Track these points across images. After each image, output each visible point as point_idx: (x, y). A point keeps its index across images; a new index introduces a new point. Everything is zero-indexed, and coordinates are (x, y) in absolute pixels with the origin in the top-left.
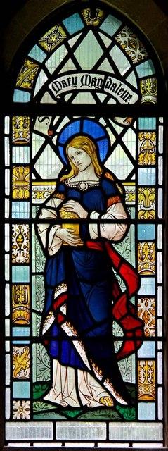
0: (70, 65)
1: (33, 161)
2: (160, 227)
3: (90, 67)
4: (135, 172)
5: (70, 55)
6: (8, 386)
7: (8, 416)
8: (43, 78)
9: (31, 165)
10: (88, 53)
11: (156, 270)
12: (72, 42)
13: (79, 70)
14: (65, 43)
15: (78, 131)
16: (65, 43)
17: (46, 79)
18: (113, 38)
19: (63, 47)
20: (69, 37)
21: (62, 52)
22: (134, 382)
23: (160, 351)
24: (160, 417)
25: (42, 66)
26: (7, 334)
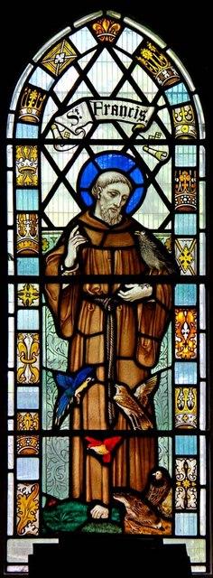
0: (83, 90)
1: (43, 205)
4: (171, 218)
5: (83, 76)
7: (10, 532)
8: (51, 108)
9: (40, 213)
11: (60, 41)
12: (83, 63)
13: (96, 96)
14: (75, 64)
16: (75, 64)
17: (55, 109)
19: (72, 69)
20: (80, 56)
21: (72, 75)
24: (203, 532)
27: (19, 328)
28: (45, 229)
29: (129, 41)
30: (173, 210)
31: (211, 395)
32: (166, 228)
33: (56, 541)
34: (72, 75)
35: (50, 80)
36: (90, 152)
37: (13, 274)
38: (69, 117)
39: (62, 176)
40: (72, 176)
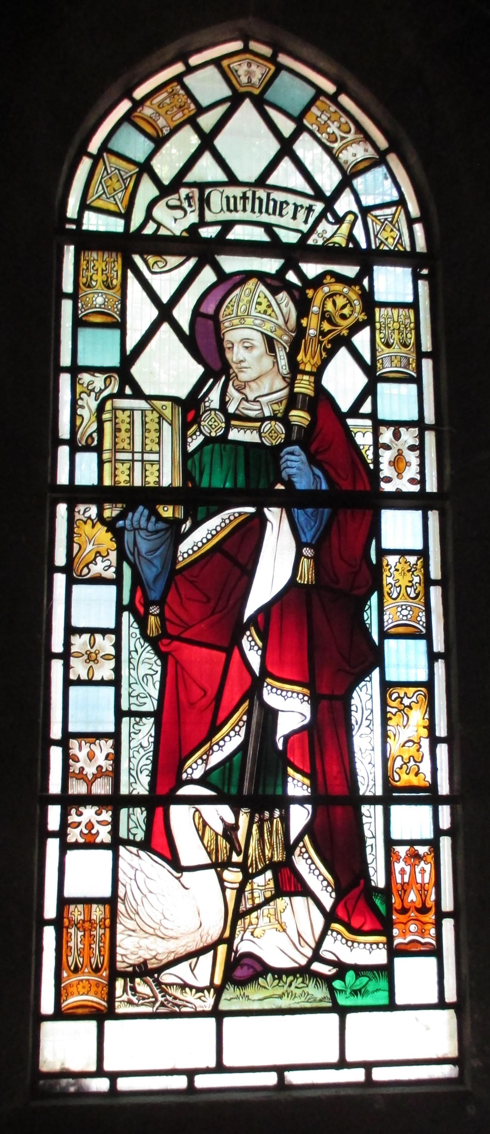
1: (128, 359)
4: (369, 391)
5: (207, 142)
7: (47, 1006)
8: (147, 191)
9: (124, 371)
12: (207, 121)
13: (233, 180)
16: (192, 121)
19: (187, 131)
20: (201, 110)
21: (187, 140)
23: (427, 355)
24: (451, 996)
25: (145, 168)
27: (68, 893)
30: (374, 376)
31: (338, 1098)
32: (363, 410)
34: (187, 140)
36: (217, 269)
37: (430, 513)
39: (165, 312)
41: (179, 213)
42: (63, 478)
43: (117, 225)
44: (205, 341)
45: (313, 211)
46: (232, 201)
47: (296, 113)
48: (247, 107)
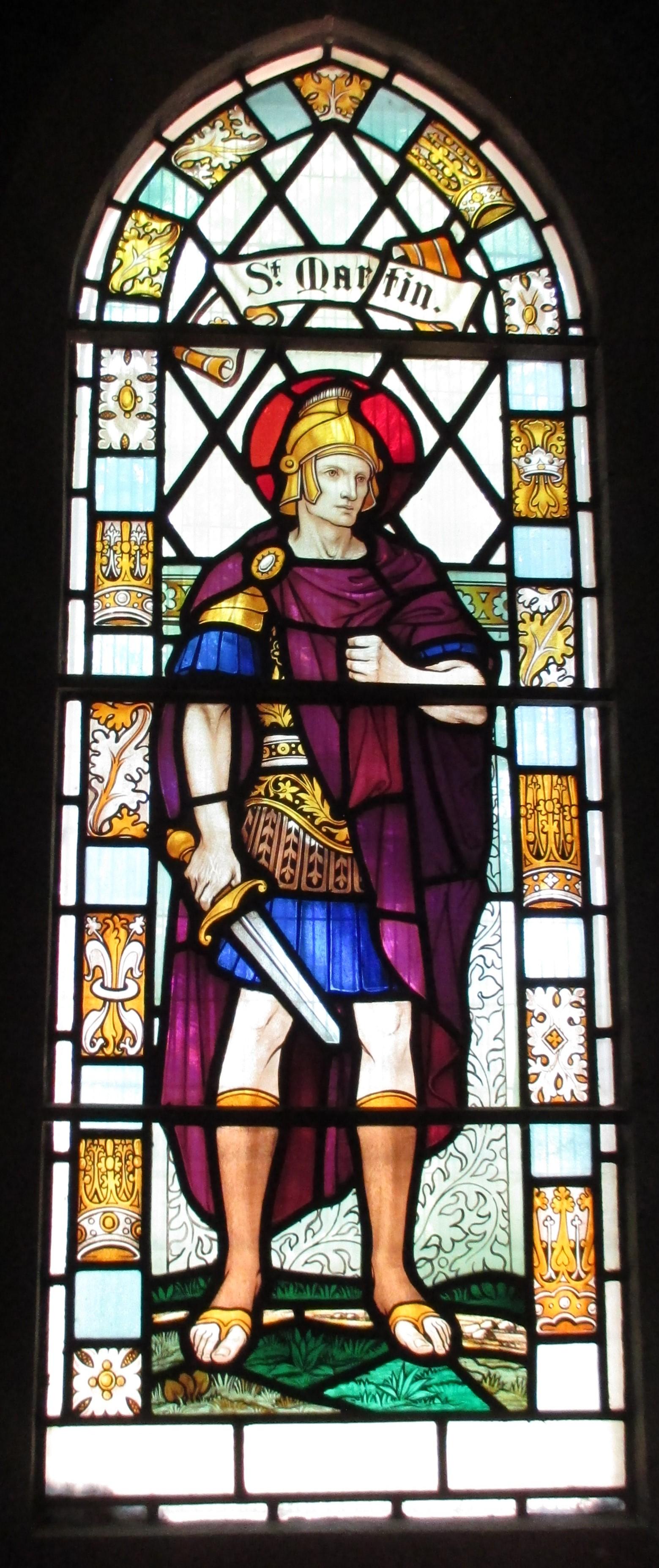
1: (166, 501)
2: (591, 715)
3: (341, 239)
4: (503, 536)
5: (276, 194)
6: (58, 1280)
7: (54, 1406)
9: (159, 521)
10: (333, 195)
12: (277, 163)
13: (311, 244)
15: (239, 577)
18: (400, 155)
19: (248, 177)
20: (273, 144)
21: (248, 191)
22: (519, 1269)
24: (617, 1401)
25: (187, 229)
26: (62, 1095)
28: (170, 561)
29: (391, 120)
30: (510, 518)
33: (155, 1042)
35: (196, 199)
36: (287, 368)
38: (250, 273)
39: (217, 430)
40: (236, 433)
41: (259, 285)
42: (75, 666)
43: (149, 315)
44: (265, 471)
45: (397, 278)
46: (420, 300)
47: (398, 145)
48: (333, 142)
